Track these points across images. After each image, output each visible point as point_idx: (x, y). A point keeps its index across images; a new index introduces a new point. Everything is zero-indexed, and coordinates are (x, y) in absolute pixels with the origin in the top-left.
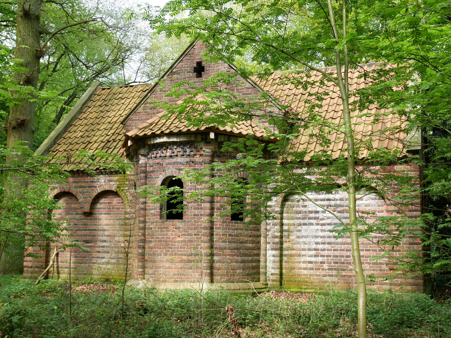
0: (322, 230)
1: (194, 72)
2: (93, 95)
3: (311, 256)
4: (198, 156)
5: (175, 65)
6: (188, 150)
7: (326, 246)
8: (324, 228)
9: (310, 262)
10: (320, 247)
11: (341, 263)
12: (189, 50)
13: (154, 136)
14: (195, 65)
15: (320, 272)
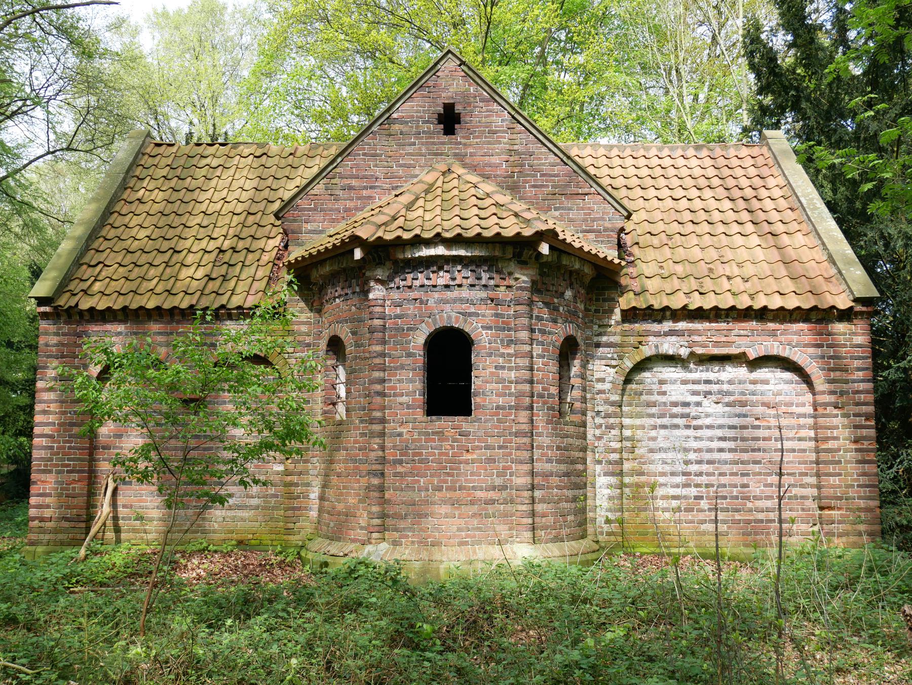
0: (696, 438)
1: (440, 123)
2: (141, 155)
3: (677, 486)
4: (503, 289)
5: (397, 106)
6: (485, 276)
7: (705, 468)
8: (699, 433)
9: (675, 498)
10: (694, 468)
11: (732, 498)
12: (427, 78)
13: (418, 241)
14: (441, 110)
15: (693, 516)
